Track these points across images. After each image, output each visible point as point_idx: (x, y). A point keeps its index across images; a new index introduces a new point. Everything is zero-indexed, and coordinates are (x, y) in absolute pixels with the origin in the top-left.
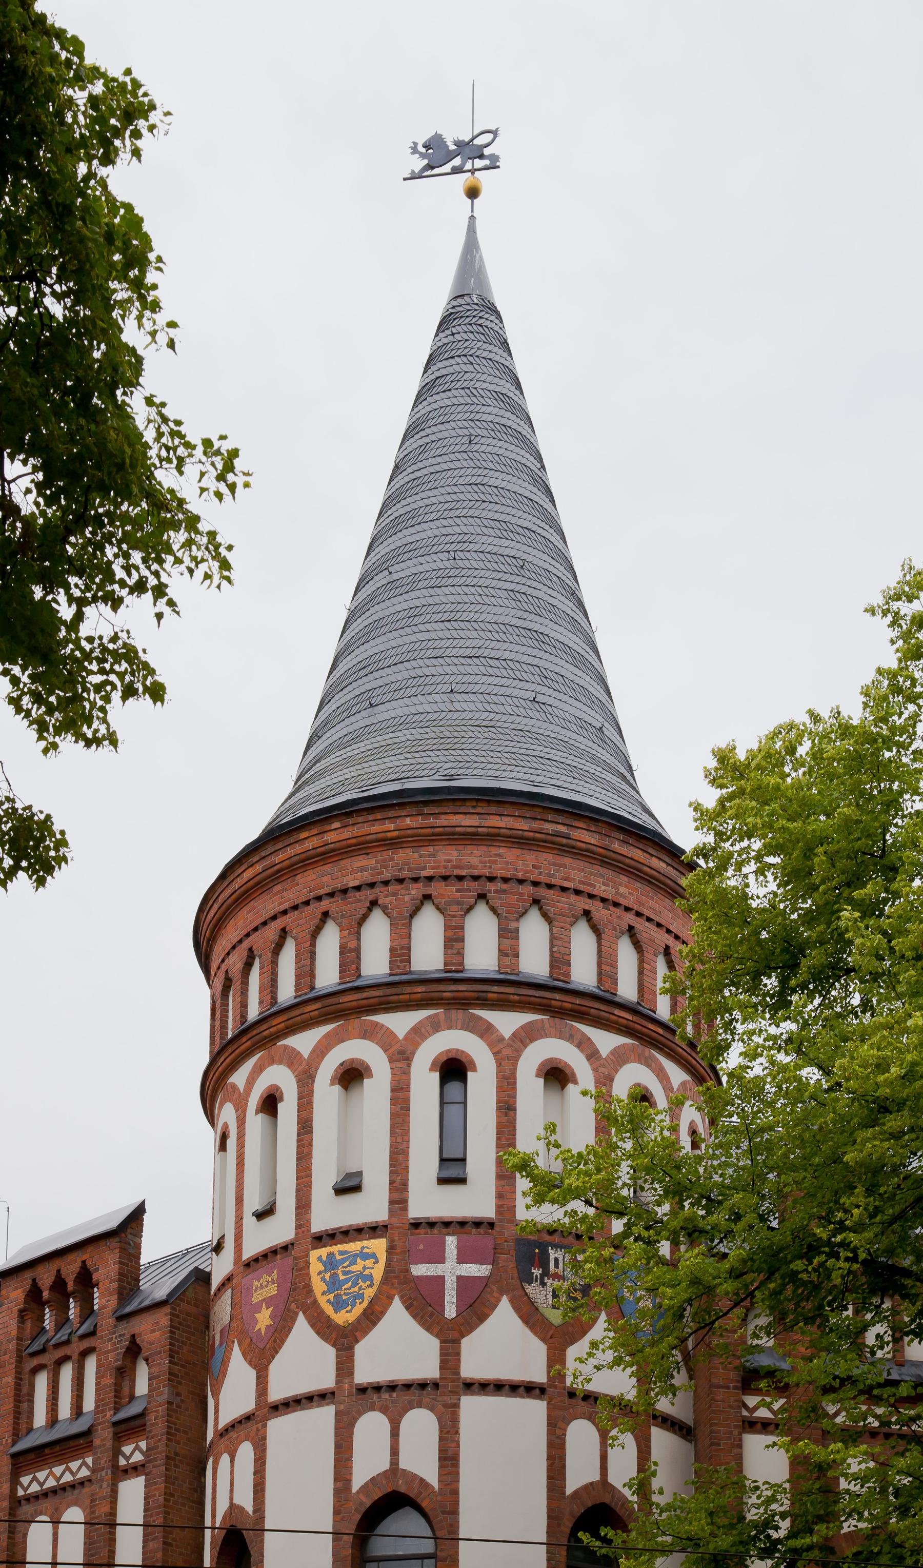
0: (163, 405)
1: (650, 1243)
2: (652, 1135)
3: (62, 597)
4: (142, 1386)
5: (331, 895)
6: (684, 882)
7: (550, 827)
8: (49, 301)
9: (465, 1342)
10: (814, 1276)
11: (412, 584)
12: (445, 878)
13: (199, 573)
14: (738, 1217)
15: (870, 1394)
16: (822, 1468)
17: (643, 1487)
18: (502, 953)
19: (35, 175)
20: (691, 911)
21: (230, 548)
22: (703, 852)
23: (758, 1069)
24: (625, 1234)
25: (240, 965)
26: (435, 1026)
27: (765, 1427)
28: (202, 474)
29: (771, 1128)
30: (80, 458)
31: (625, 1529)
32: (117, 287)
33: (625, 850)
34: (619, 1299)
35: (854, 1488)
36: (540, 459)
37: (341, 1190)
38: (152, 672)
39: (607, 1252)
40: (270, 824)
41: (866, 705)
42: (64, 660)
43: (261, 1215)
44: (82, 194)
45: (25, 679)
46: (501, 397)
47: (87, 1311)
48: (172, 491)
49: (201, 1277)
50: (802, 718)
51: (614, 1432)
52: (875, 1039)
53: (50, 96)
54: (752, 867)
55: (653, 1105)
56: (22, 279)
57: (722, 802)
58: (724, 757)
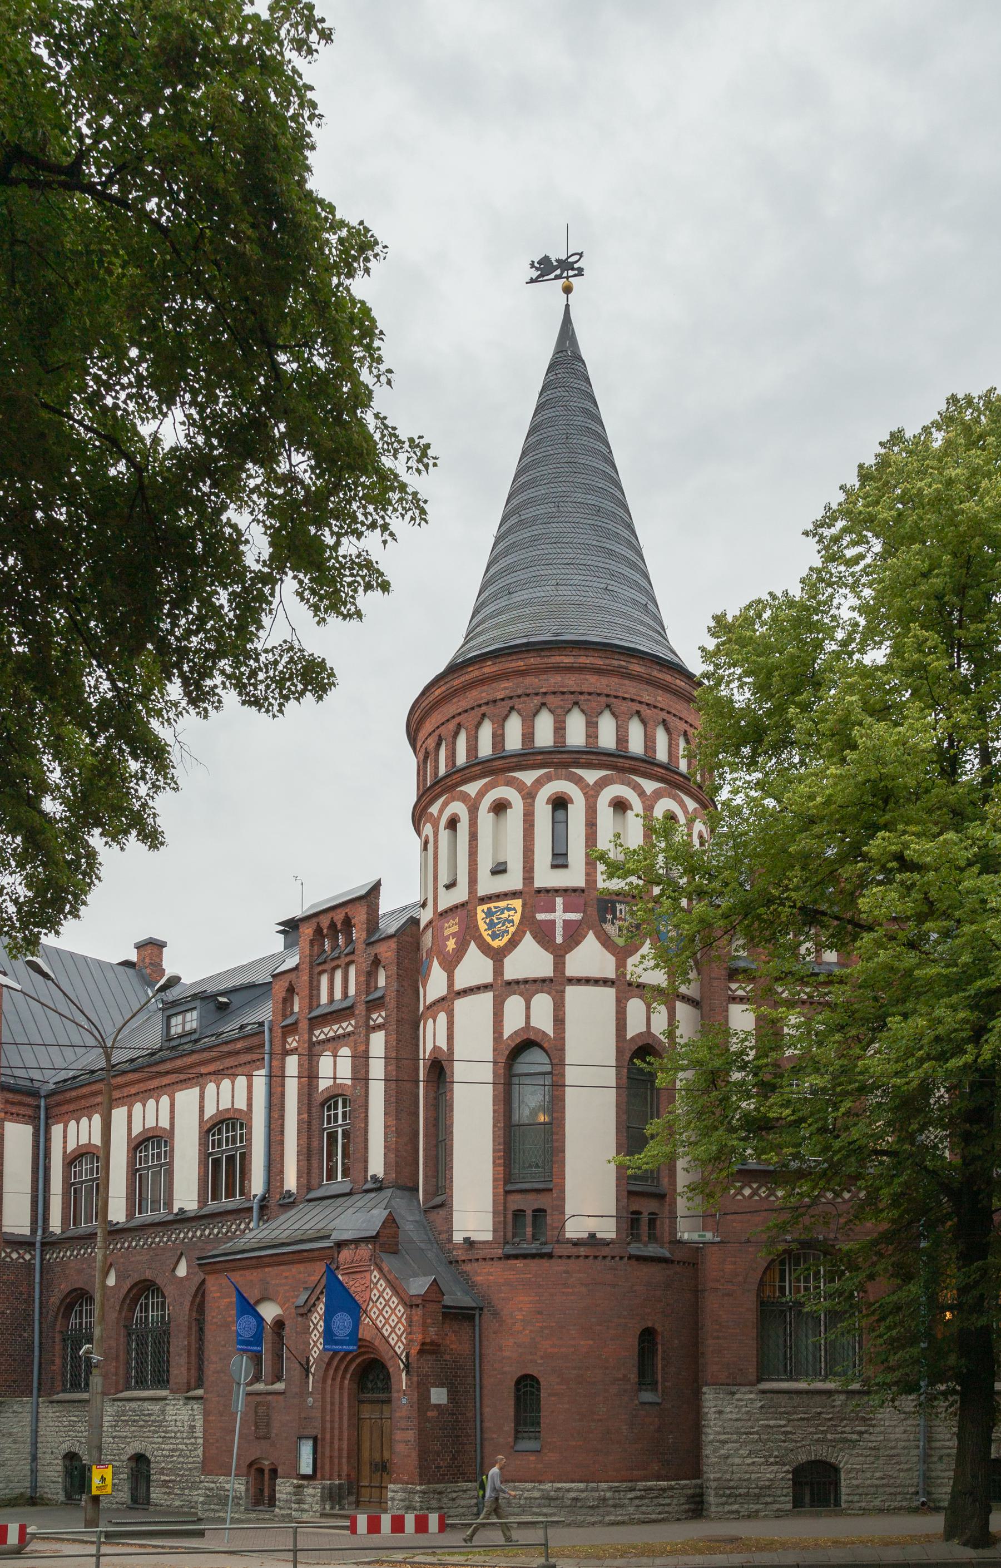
0: (385, 418)
1: (675, 899)
2: (677, 839)
3: (327, 532)
4: (382, 982)
5: (487, 704)
6: (695, 693)
7: (615, 663)
8: (315, 359)
9: (568, 956)
10: (771, 917)
11: (534, 521)
12: (554, 693)
13: (408, 517)
14: (727, 884)
15: (802, 981)
16: (774, 1022)
17: (671, 1034)
18: (588, 736)
19: (307, 285)
20: (700, 710)
21: (425, 502)
22: (706, 675)
23: (739, 800)
24: (661, 895)
25: (433, 745)
26: (548, 779)
27: (741, 1000)
28: (409, 459)
29: (746, 833)
30: (336, 450)
31: (661, 1057)
32: (359, 352)
33: (660, 675)
34: (658, 932)
35: (792, 1032)
36: (609, 447)
37: (495, 872)
38: (382, 574)
39: (650, 905)
40: (454, 659)
41: (803, 589)
42: (330, 569)
43: (448, 887)
44: (335, 295)
45: (306, 581)
46: (586, 411)
47: (349, 941)
48: (390, 469)
49: (414, 922)
50: (766, 597)
51: (654, 1005)
52: (808, 782)
53: (316, 238)
54: (736, 684)
55: (677, 821)
56: (300, 346)
57: (718, 646)
58: (719, 619)
